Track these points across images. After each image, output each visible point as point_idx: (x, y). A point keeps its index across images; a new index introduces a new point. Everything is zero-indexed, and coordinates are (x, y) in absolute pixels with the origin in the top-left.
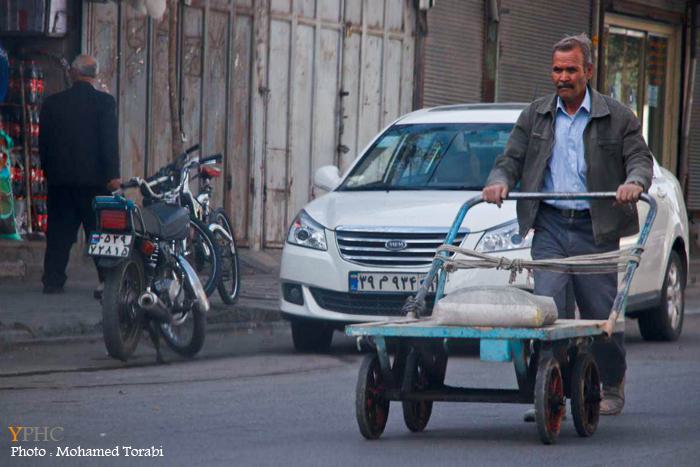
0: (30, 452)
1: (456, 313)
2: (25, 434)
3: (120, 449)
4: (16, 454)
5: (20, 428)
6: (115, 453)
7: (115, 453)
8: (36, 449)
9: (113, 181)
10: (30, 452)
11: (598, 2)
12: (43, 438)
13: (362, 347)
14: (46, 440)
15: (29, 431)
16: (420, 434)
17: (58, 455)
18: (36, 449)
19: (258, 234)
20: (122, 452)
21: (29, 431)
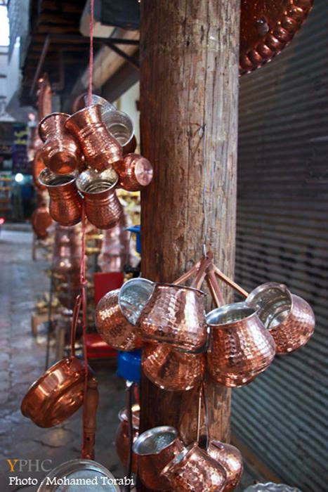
0: (25, 482)
1: (234, 60)
2: (21, 465)
3: (99, 480)
4: (14, 483)
5: (16, 461)
6: (94, 482)
7: (94, 482)
8: (30, 479)
9: (135, 238)
10: (25, 482)
11: (325, 119)
12: (35, 469)
13: (159, 289)
14: (104, 484)
15: (23, 463)
16: (40, 99)
17: (47, 484)
18: (30, 479)
19: (182, 426)
20: (100, 481)
21: (23, 463)
